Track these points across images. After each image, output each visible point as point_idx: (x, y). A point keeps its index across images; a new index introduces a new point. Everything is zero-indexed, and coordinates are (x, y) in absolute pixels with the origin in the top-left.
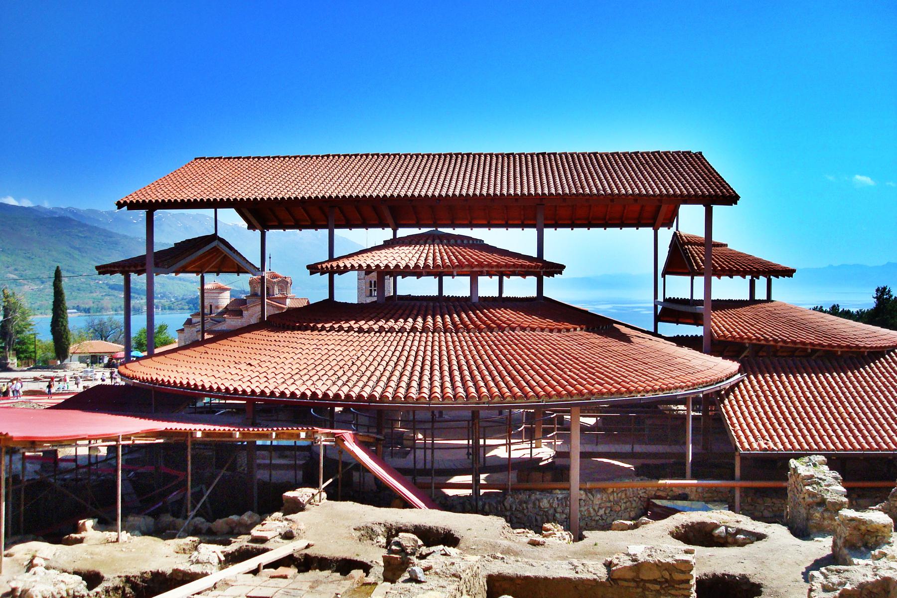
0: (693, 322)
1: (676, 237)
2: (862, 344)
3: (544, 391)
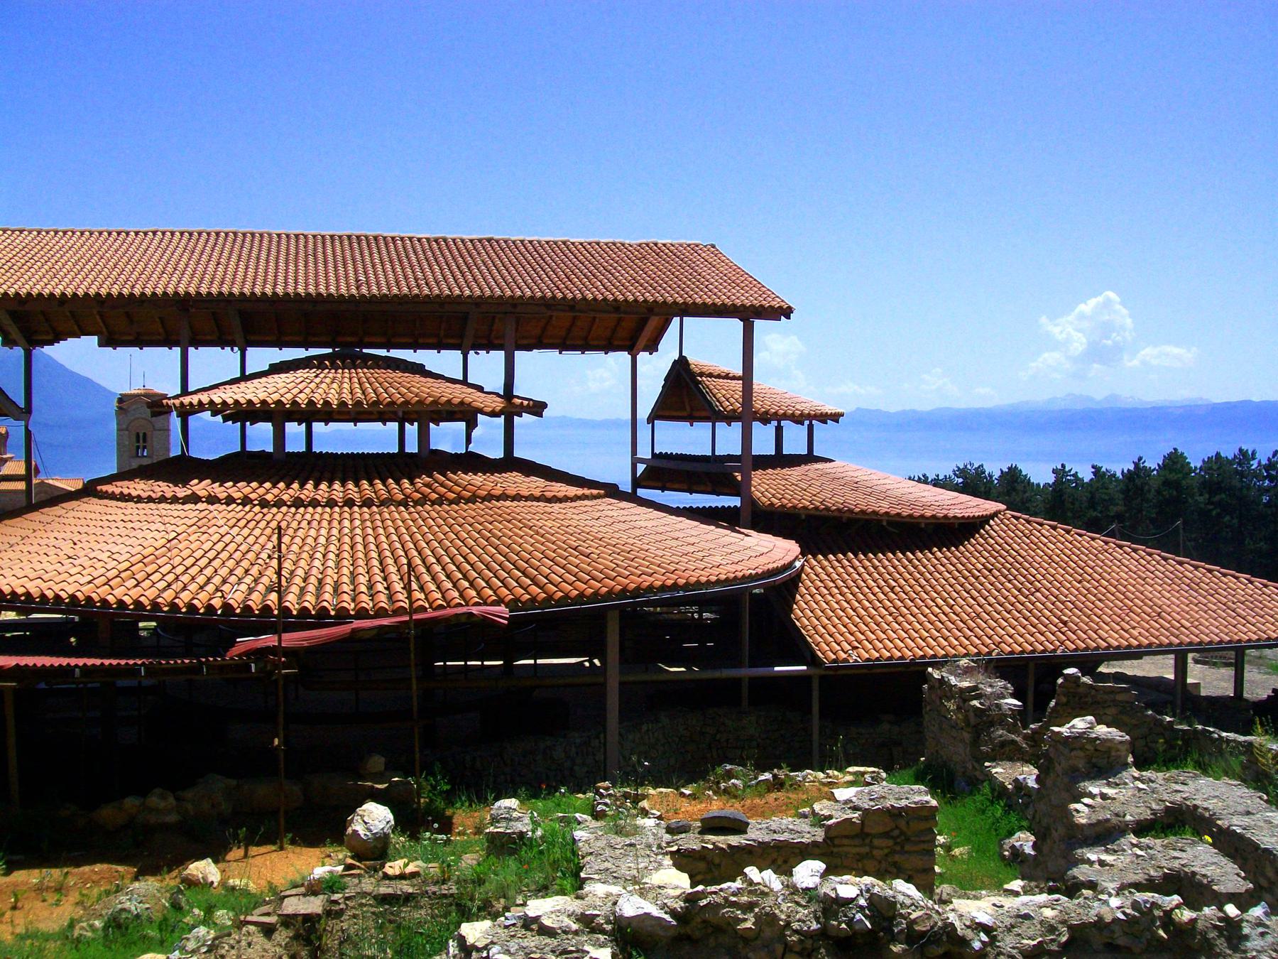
0: (685, 488)
1: (681, 365)
2: (951, 514)
3: (545, 593)
